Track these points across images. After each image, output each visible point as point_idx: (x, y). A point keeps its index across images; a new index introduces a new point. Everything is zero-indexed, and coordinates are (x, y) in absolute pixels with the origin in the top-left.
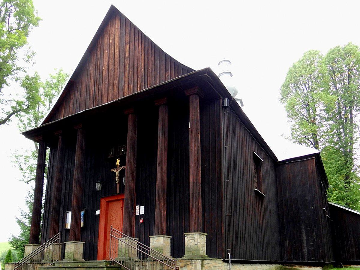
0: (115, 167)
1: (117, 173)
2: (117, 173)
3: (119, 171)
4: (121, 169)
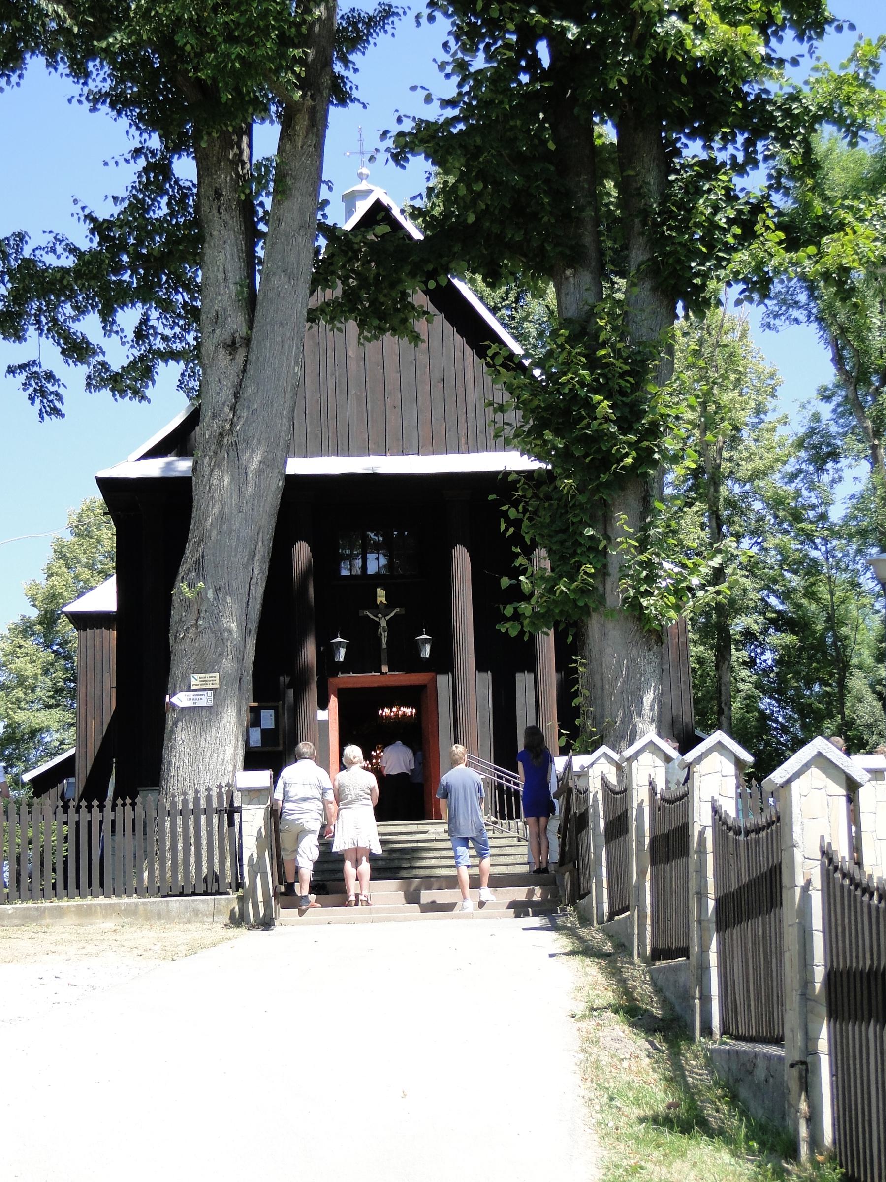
0: (372, 604)
1: (383, 623)
2: (383, 623)
3: (387, 618)
4: (392, 614)
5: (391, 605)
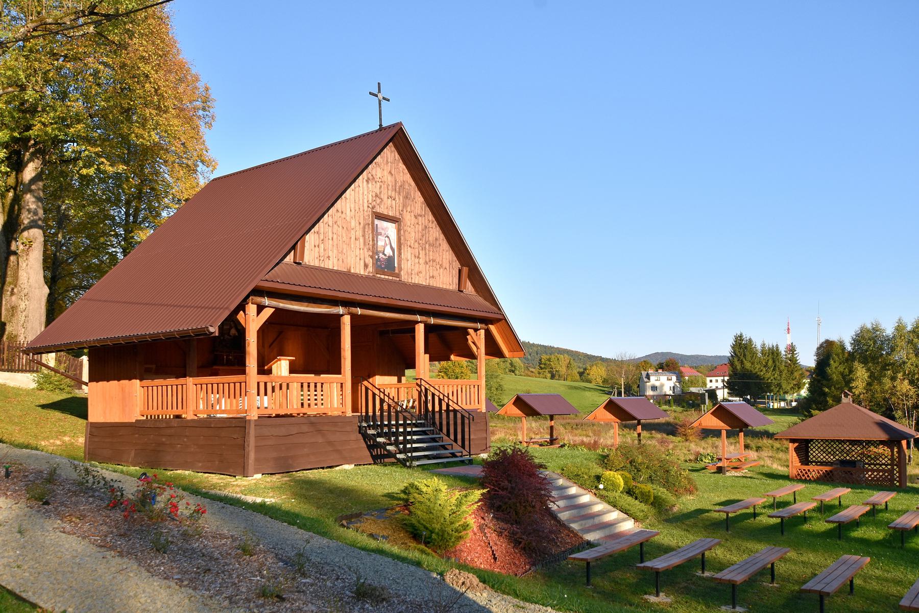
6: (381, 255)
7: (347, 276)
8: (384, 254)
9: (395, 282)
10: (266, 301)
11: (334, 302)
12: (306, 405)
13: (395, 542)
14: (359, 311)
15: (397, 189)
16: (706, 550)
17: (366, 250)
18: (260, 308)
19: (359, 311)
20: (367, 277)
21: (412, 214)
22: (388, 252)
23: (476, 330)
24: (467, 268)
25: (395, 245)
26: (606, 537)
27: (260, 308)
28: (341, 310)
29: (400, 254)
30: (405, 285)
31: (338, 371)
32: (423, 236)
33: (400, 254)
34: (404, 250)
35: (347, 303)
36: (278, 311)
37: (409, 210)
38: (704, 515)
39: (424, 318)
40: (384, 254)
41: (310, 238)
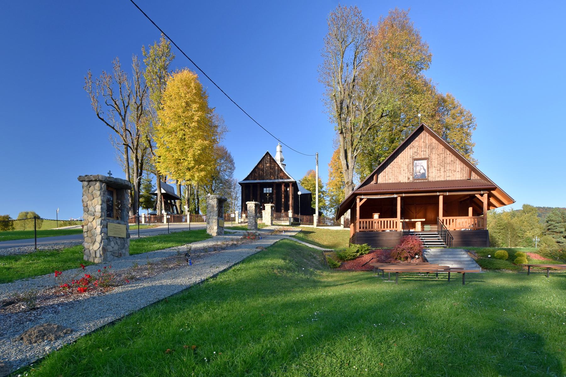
5: (269, 195)
6: (418, 173)
7: (400, 184)
8: (419, 172)
9: (426, 182)
10: (362, 197)
11: (393, 193)
12: (365, 228)
13: (369, 274)
14: (404, 195)
15: (427, 147)
16: (157, 197)
17: (409, 173)
18: (361, 200)
19: (404, 195)
20: (409, 183)
21: (436, 154)
22: (422, 171)
23: (482, 195)
24: (225, 223)
25: (426, 168)
26: (219, 216)
27: (361, 200)
28: (395, 196)
29: (428, 171)
30: (430, 182)
31: (396, 217)
32: (443, 161)
33: (428, 171)
34: (431, 169)
35: (397, 193)
36: (368, 199)
37: (434, 153)
38: (133, 194)
39: (442, 193)
40: (419, 172)
41: (381, 175)
